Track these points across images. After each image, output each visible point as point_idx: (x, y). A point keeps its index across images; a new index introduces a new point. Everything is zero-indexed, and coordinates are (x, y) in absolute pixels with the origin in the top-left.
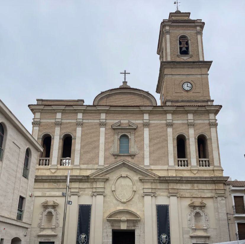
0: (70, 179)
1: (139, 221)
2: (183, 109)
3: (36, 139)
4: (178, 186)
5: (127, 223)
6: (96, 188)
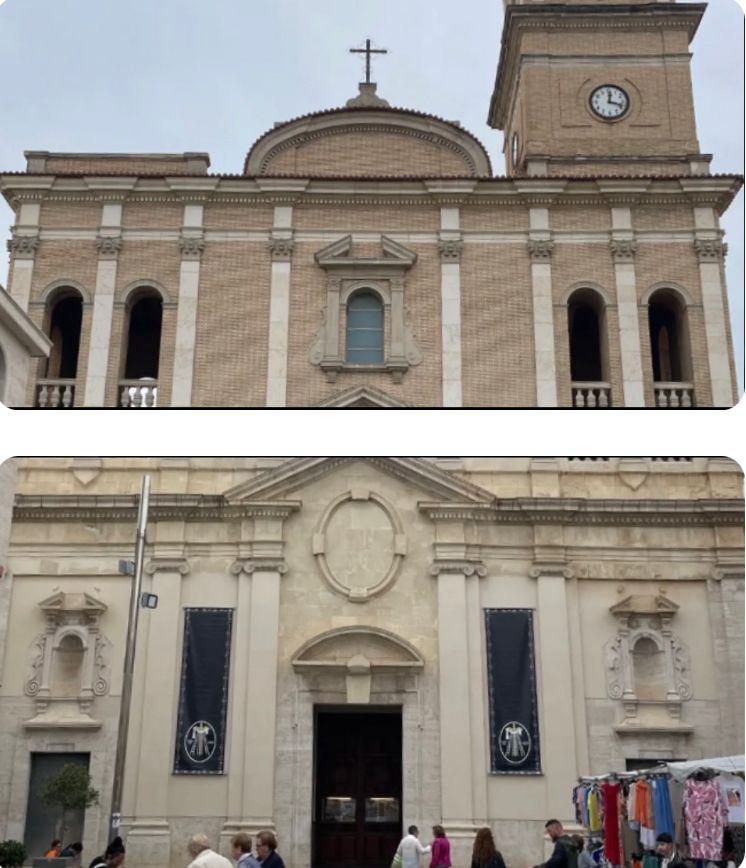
0: (150, 508)
1: (418, 674)
2: (593, 189)
3: (25, 307)
4: (570, 537)
5: (373, 678)
6: (250, 543)
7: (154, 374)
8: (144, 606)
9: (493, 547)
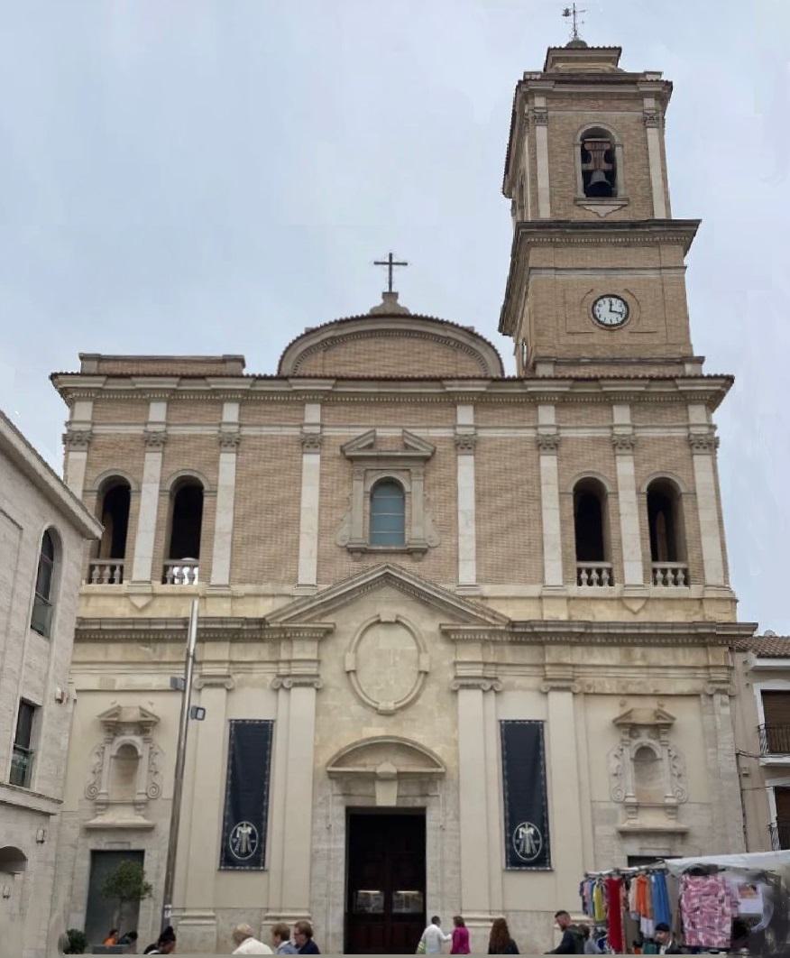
0: (198, 629)
1: (440, 779)
2: (597, 387)
3: (79, 494)
4: (577, 655)
5: (399, 783)
6: (289, 662)
7: (196, 555)
8: (192, 719)
9: (508, 665)
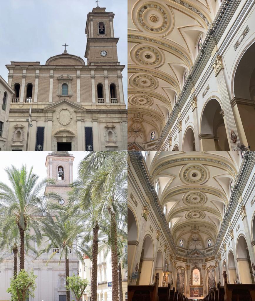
0: (31, 111)
3: (11, 86)
4: (98, 115)
6: (47, 116)
7: (31, 97)
